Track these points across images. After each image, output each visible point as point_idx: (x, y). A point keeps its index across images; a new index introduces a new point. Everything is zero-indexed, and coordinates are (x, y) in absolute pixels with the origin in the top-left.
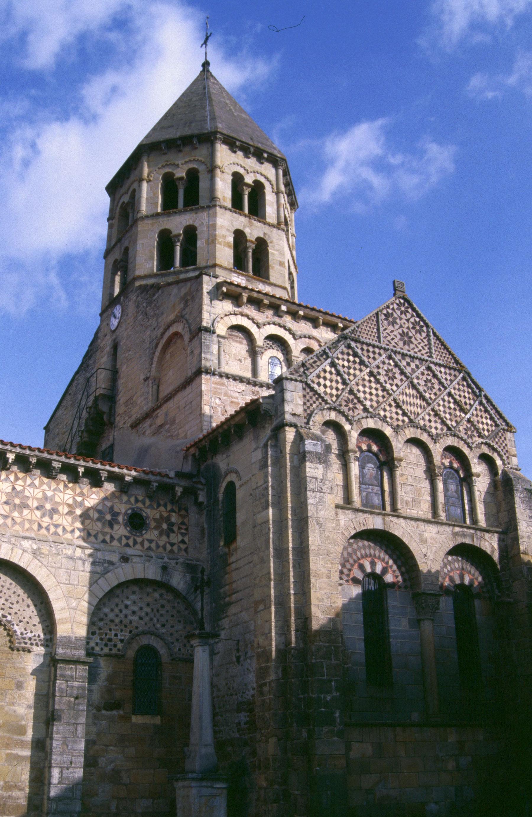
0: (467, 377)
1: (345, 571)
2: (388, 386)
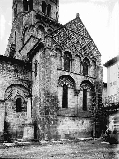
2: (73, 41)
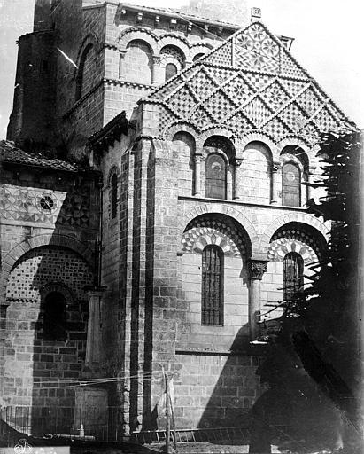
0: (314, 87)
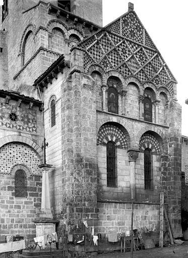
1: (100, 140)
